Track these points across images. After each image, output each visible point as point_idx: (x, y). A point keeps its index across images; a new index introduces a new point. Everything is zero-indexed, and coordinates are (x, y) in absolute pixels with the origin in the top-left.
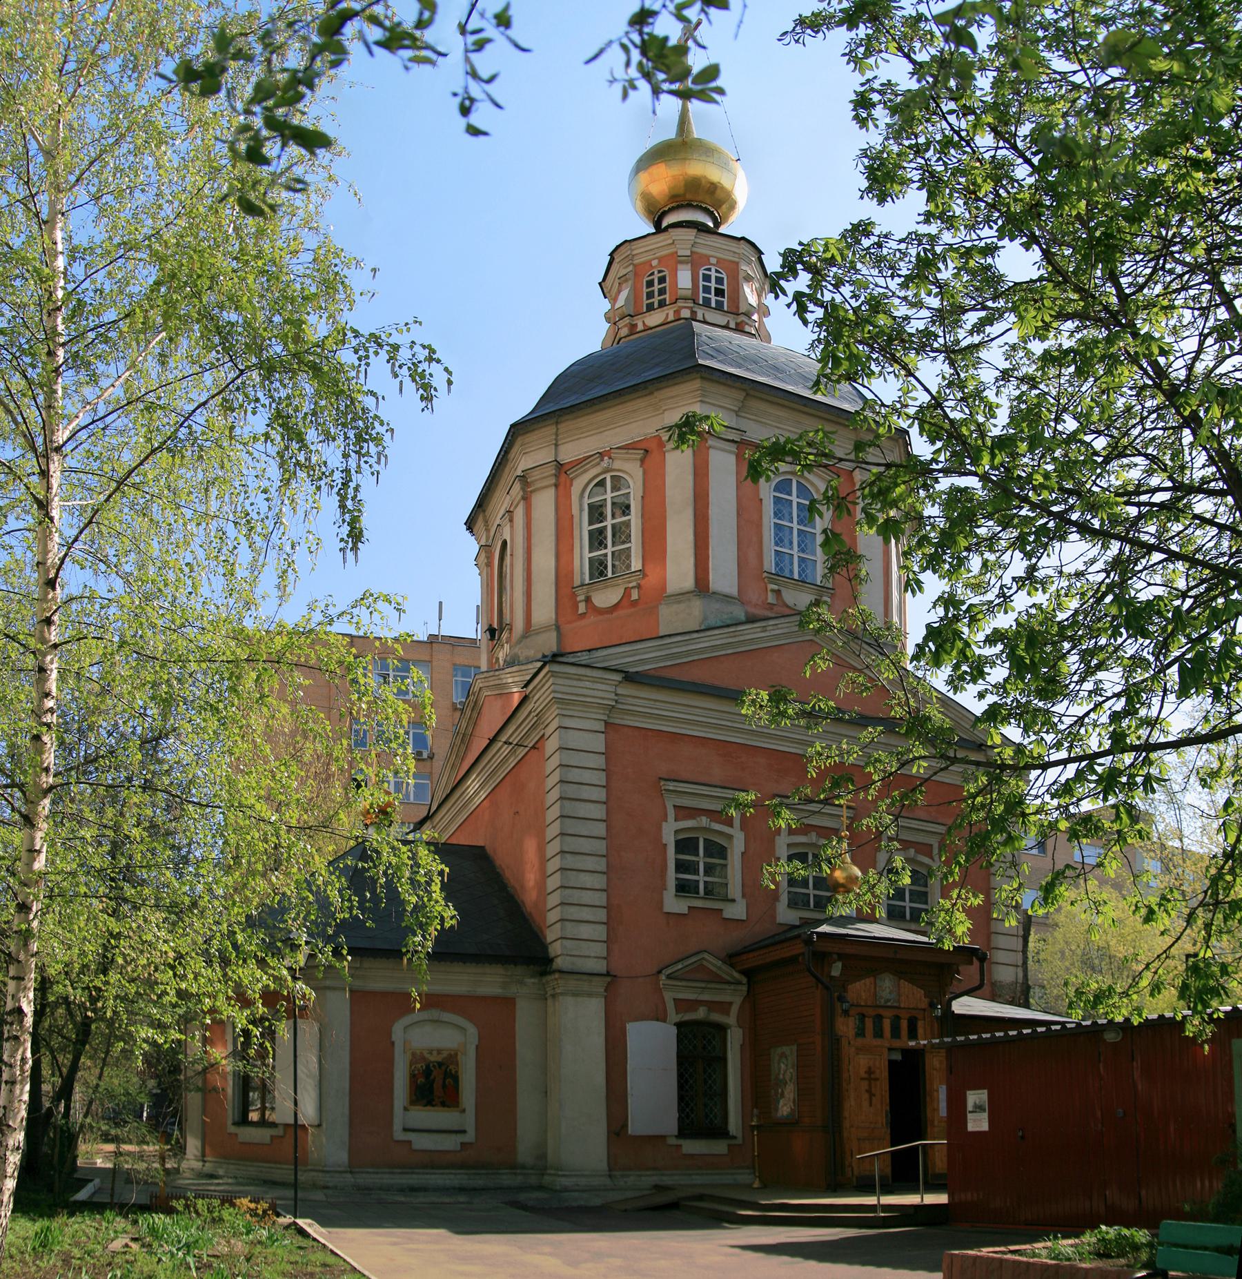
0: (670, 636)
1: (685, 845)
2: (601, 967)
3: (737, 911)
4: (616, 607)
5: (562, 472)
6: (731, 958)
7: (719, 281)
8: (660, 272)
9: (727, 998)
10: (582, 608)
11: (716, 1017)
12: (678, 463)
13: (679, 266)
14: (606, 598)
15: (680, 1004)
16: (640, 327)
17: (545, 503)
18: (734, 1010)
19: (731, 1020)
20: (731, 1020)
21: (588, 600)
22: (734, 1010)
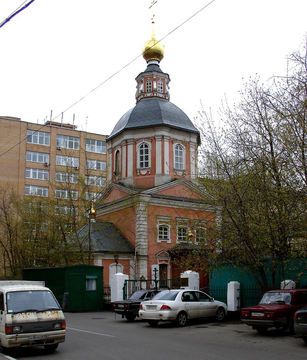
0: (127, 155)
1: (161, 228)
2: (147, 255)
3: (169, 242)
4: (145, 175)
5: (135, 142)
6: (169, 252)
7: (161, 84)
8: (150, 81)
9: (168, 259)
10: (138, 174)
11: (166, 263)
12: (158, 144)
13: (154, 81)
14: (144, 172)
15: (160, 261)
16: (145, 96)
17: (130, 148)
18: (169, 261)
19: (168, 264)
20: (168, 264)
21: (140, 172)
22: (169, 261)
